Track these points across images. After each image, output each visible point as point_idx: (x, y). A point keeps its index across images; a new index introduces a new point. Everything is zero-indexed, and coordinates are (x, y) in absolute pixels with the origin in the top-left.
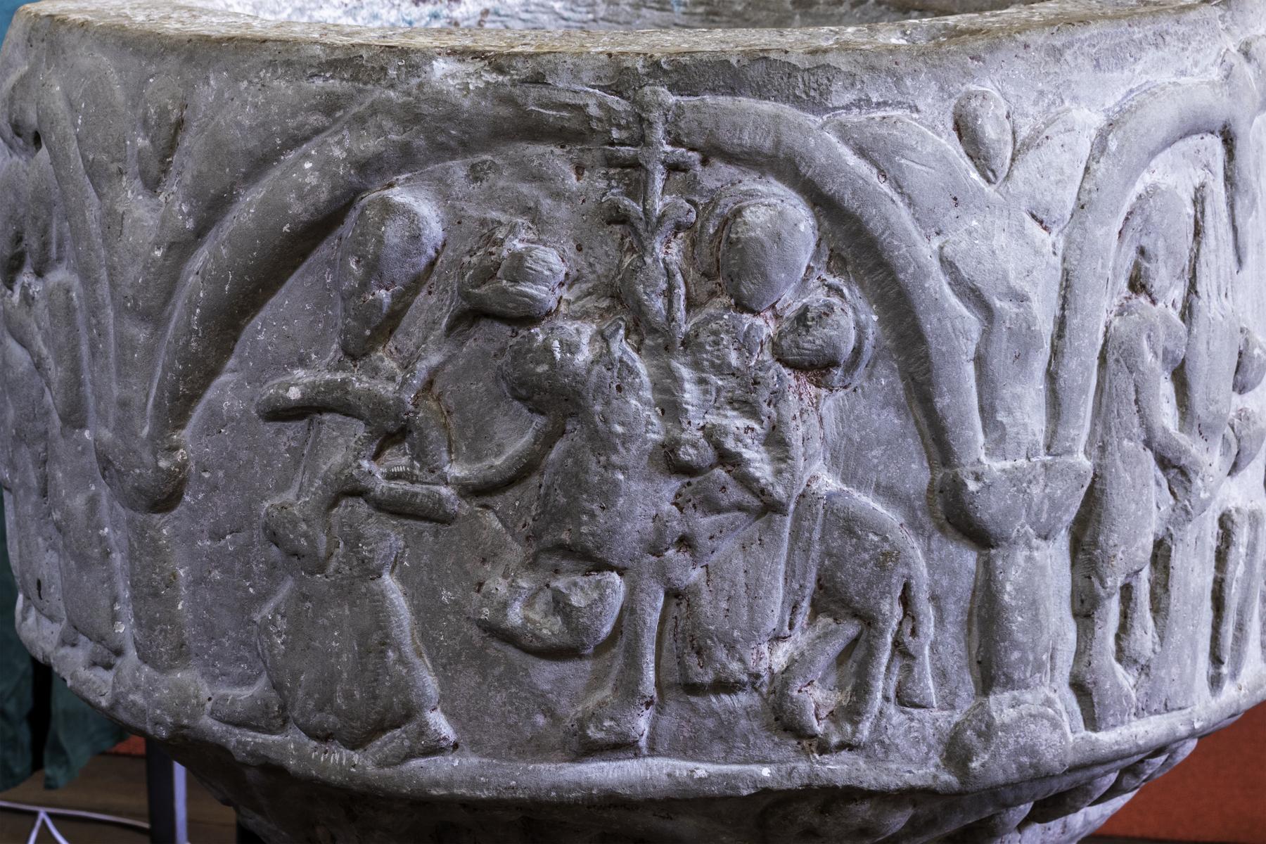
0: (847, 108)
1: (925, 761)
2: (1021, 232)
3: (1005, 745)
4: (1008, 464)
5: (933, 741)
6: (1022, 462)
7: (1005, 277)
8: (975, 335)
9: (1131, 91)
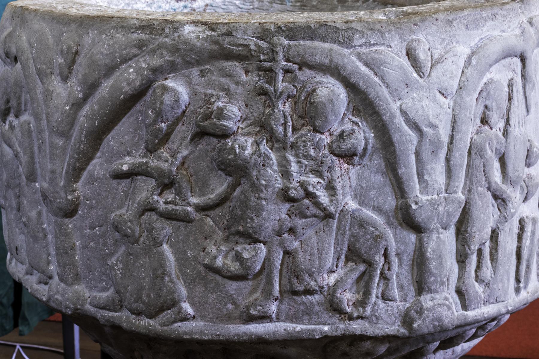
0: (361, 46)
1: (394, 324)
2: (435, 99)
3: (428, 317)
4: (429, 198)
5: (397, 315)
6: (435, 196)
7: (428, 118)
8: (415, 143)
9: (482, 39)
